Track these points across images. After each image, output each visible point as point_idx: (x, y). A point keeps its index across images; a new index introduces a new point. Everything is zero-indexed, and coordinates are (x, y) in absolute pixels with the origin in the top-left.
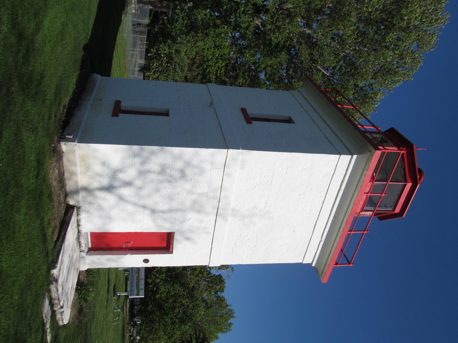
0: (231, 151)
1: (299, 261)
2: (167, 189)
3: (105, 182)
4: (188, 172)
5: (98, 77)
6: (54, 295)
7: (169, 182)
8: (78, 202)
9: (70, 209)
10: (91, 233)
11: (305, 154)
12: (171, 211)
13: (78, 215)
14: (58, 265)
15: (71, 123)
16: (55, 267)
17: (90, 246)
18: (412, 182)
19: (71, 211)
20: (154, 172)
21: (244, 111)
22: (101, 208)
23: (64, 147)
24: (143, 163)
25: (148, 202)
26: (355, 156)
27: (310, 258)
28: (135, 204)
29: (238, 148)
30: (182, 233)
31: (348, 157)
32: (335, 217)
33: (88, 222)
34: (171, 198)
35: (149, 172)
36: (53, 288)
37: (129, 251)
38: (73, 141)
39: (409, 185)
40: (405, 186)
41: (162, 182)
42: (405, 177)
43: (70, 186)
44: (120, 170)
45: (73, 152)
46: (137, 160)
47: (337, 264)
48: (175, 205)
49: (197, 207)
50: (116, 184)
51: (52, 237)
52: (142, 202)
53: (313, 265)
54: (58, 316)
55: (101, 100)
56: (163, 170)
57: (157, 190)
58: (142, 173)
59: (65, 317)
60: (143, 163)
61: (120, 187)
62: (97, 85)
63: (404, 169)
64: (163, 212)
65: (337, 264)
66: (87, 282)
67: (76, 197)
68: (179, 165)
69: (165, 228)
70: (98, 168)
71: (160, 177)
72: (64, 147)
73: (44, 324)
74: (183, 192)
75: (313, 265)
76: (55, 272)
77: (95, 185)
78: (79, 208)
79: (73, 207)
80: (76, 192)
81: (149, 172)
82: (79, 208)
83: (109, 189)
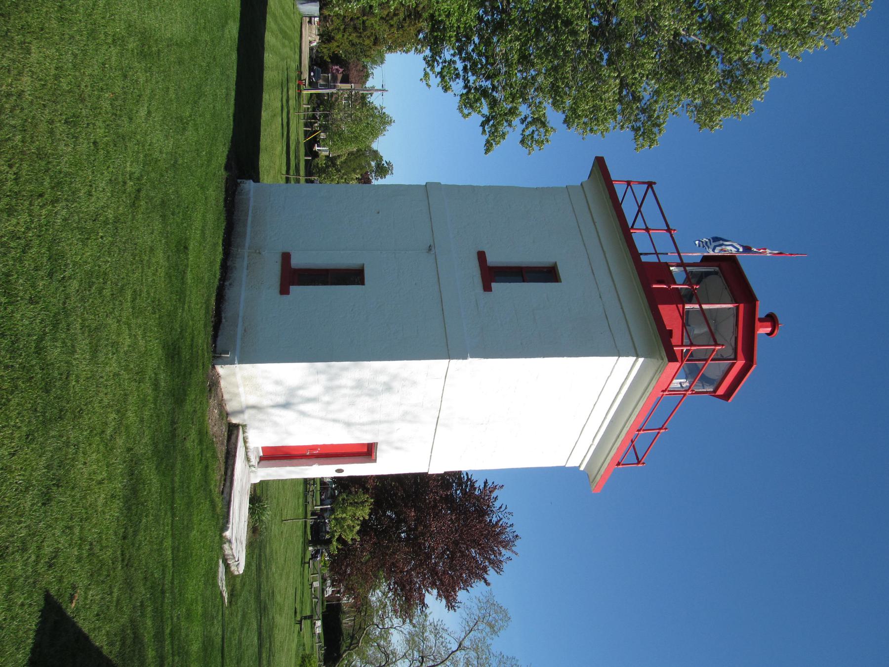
0: (453, 362)
1: (561, 463)
2: (366, 402)
3: (281, 400)
4: (396, 385)
5: (249, 185)
6: (227, 551)
7: (370, 395)
8: (244, 420)
9: (233, 430)
10: (263, 448)
11: (565, 358)
12: (373, 423)
13: (244, 432)
14: (230, 526)
15: (224, 320)
16: (226, 529)
17: (261, 454)
18: (746, 359)
19: (235, 432)
20: (345, 387)
21: (481, 256)
22: (276, 424)
23: (221, 370)
24: (331, 379)
25: (342, 416)
26: (641, 360)
27: (578, 458)
28: (322, 419)
29: (465, 358)
30: (389, 443)
31: (632, 359)
32: (611, 421)
33: (257, 438)
34: (372, 411)
35: (339, 387)
36: (226, 546)
37: (315, 460)
38: (232, 363)
39: (740, 363)
40: (733, 365)
41: (358, 396)
42: (735, 350)
43: (229, 407)
44: (300, 388)
45: (234, 374)
46: (323, 378)
47: (619, 464)
48: (377, 417)
49: (408, 417)
50: (295, 400)
51: (216, 476)
52: (330, 416)
53: (582, 468)
54: (233, 568)
55: (260, 253)
56: (359, 385)
57: (352, 404)
58: (329, 389)
59: (239, 567)
60: (331, 379)
61: (300, 403)
62: (251, 209)
63: (736, 338)
64: (363, 424)
65: (619, 464)
66: (258, 496)
67: (241, 416)
68: (383, 378)
69: (366, 439)
70: (271, 388)
71: (357, 392)
72: (221, 370)
73: (221, 593)
74: (388, 404)
75: (582, 468)
76: (227, 534)
77: (265, 402)
78: (244, 426)
79: (237, 426)
80: (241, 412)
81: (339, 387)
82: (244, 426)
83: (286, 406)
